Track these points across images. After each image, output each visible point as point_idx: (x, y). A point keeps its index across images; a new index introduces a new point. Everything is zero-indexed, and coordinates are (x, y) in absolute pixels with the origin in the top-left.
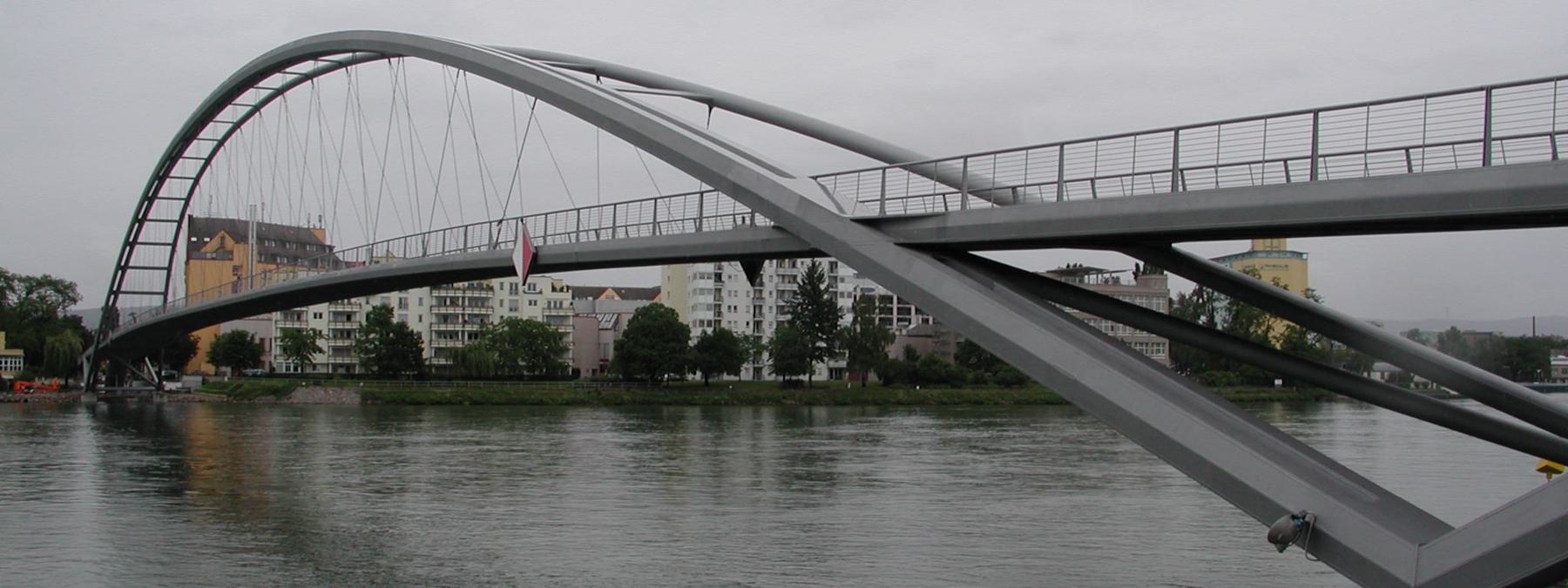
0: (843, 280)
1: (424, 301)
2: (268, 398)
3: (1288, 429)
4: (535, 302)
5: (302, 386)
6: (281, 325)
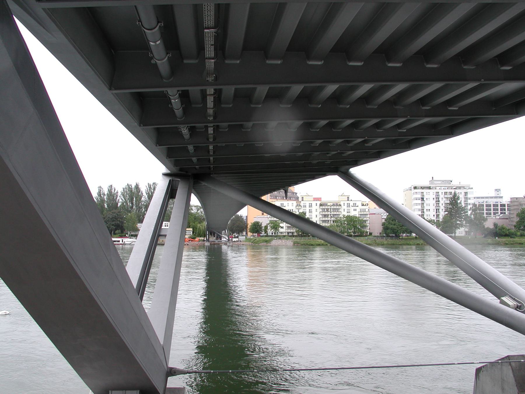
0: (470, 199)
1: (318, 210)
2: (264, 243)
3: (338, 249)
4: (356, 209)
5: (275, 239)
6: (270, 219)
